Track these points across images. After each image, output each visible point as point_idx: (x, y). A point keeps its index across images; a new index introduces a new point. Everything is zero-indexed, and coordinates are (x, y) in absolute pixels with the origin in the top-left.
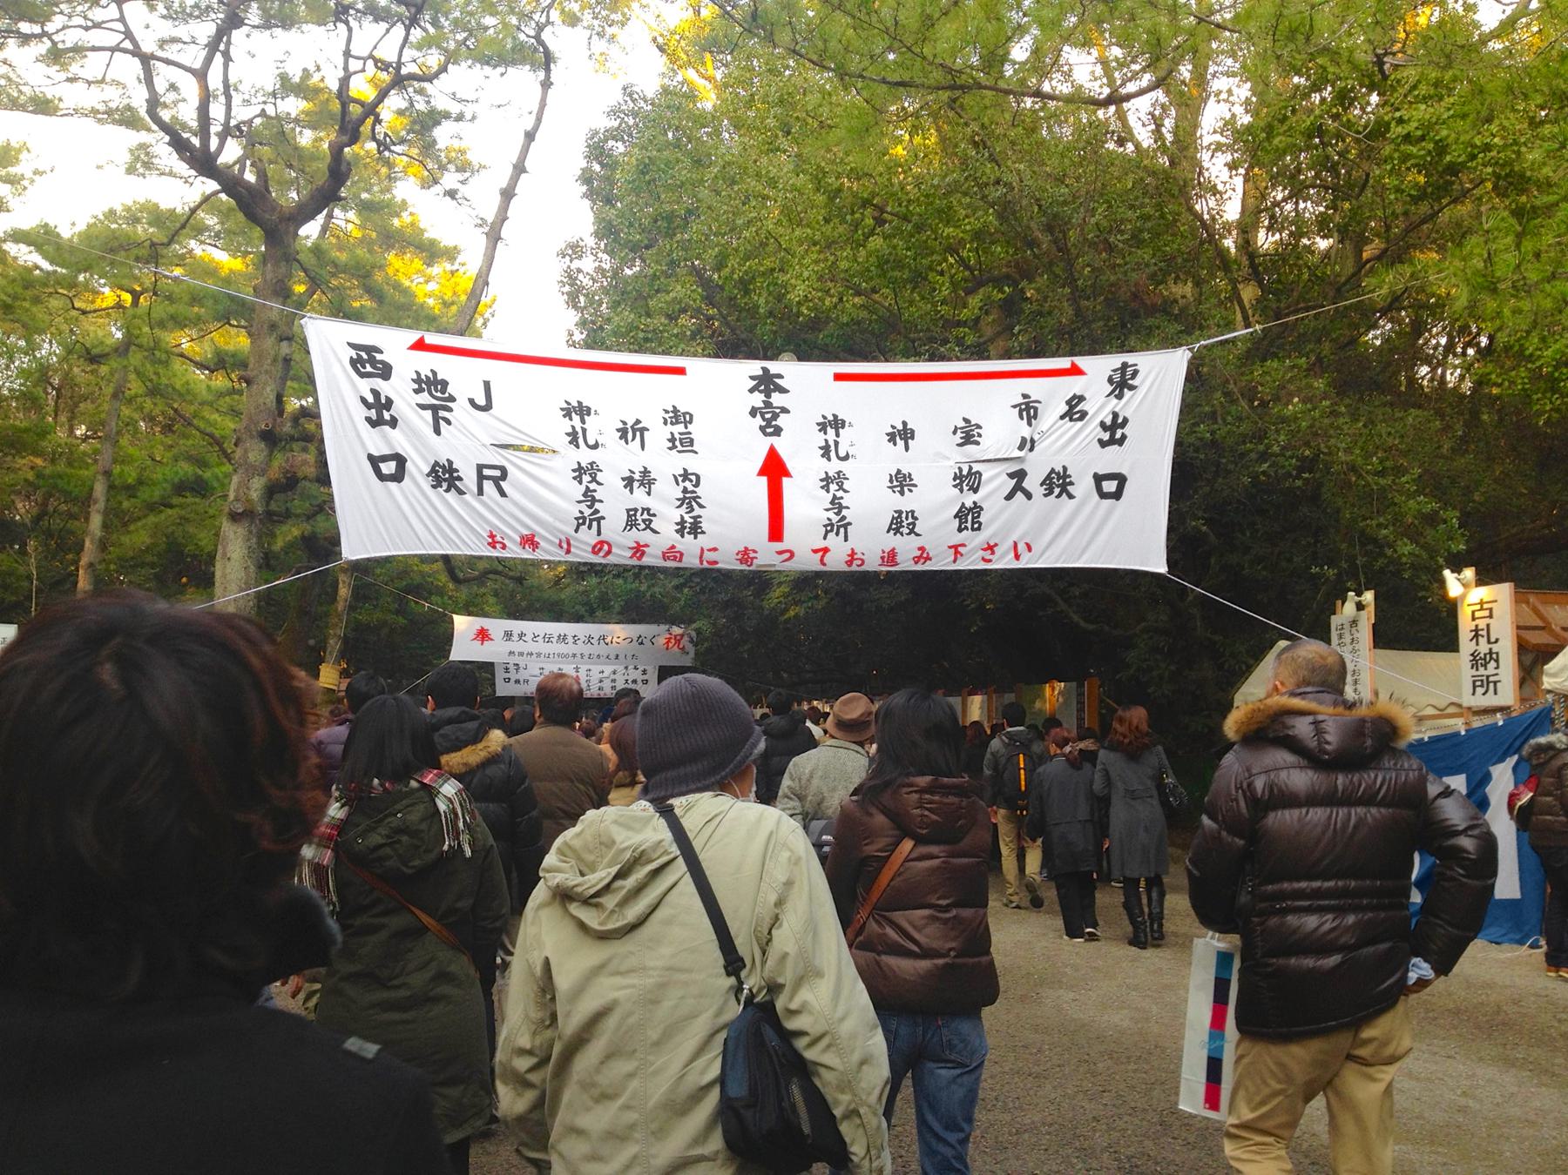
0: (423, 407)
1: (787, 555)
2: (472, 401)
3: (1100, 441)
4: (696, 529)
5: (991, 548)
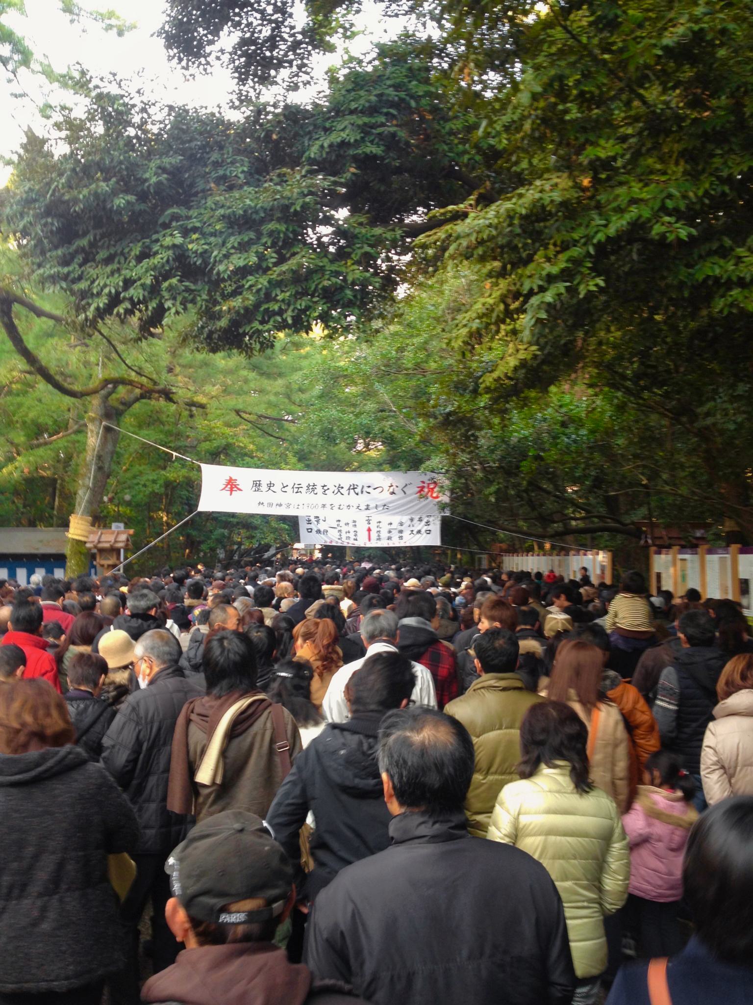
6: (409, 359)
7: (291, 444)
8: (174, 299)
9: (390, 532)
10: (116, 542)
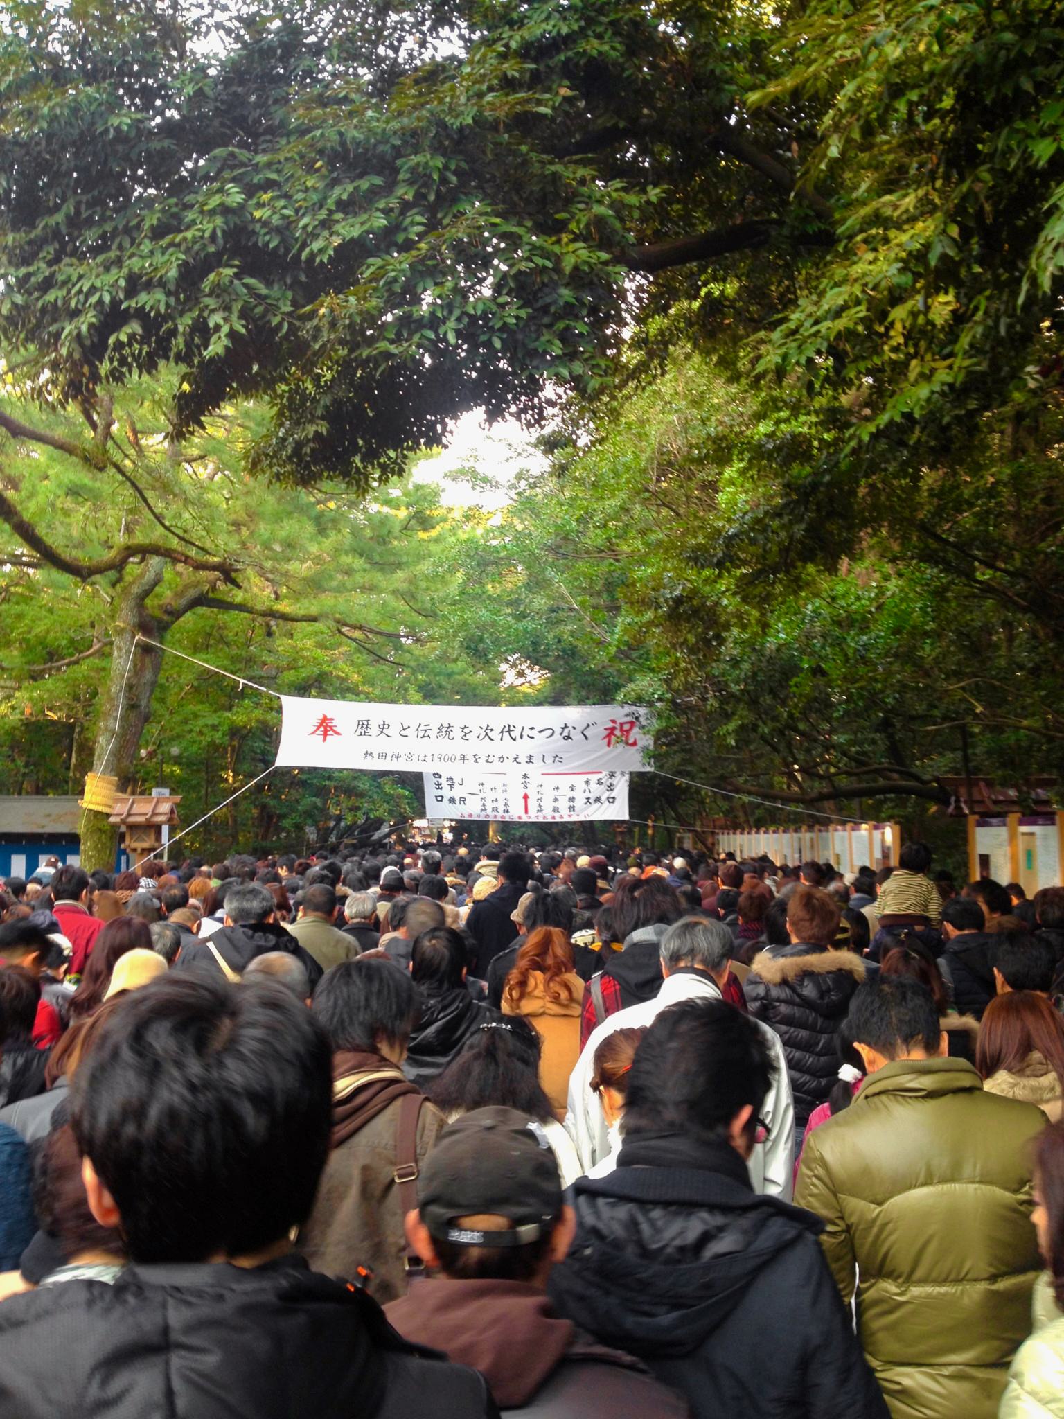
6: (594, 538)
7: (414, 672)
8: (227, 308)
9: (556, 800)
10: (154, 814)
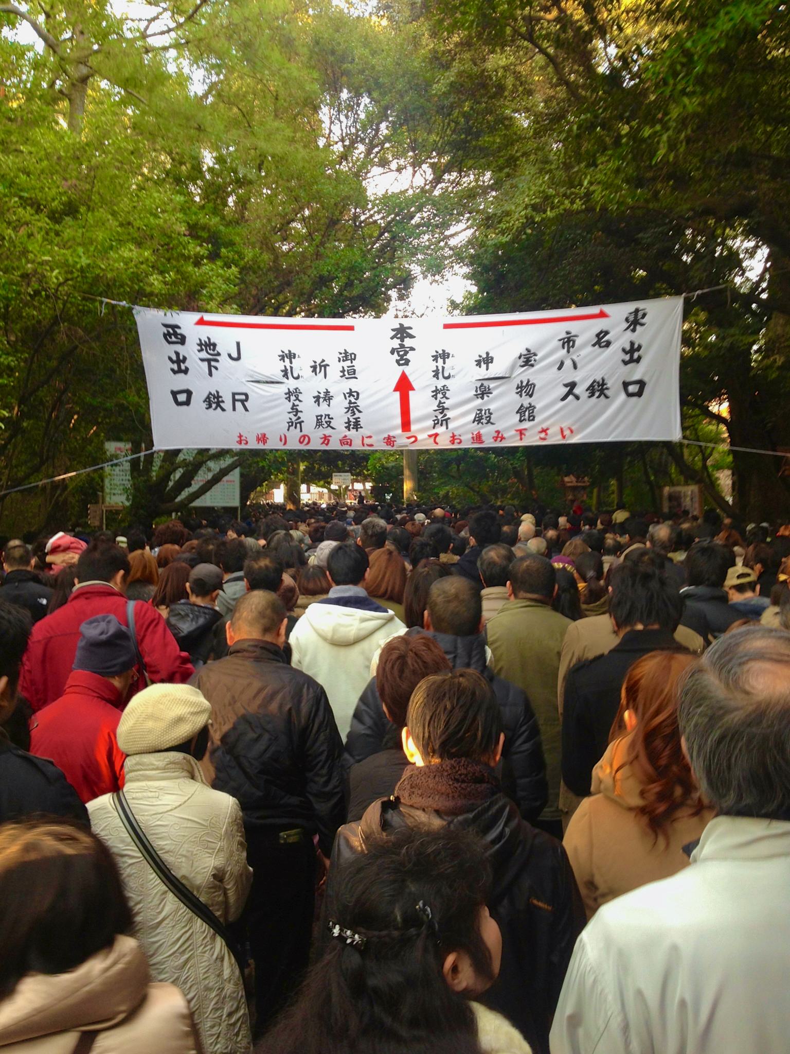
0: (202, 360)
1: (413, 439)
2: (230, 356)
3: (623, 361)
4: (357, 426)
5: (544, 431)
9: (483, 392)
